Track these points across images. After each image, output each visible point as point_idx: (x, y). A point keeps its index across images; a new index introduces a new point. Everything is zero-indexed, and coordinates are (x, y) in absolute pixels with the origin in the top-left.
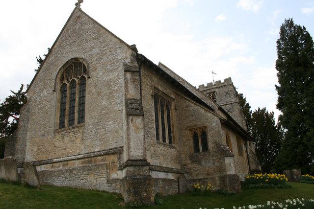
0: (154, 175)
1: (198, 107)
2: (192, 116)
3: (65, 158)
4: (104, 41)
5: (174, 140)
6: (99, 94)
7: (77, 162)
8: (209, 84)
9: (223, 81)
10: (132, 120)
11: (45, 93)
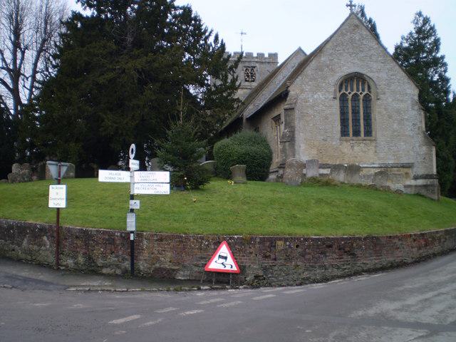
6: (390, 117)
8: (248, 53)
9: (266, 56)
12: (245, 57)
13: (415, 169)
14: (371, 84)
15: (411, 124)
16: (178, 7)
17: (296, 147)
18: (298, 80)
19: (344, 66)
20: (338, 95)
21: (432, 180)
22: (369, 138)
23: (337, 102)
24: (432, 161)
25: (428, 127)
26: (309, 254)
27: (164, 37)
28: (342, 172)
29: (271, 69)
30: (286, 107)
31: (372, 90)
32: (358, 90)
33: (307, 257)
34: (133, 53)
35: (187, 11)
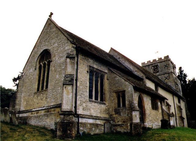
0: (81, 120)
1: (121, 78)
2: (117, 84)
3: (37, 109)
4: (60, 39)
5: (105, 99)
7: (43, 112)
10: (65, 88)
11: (31, 70)
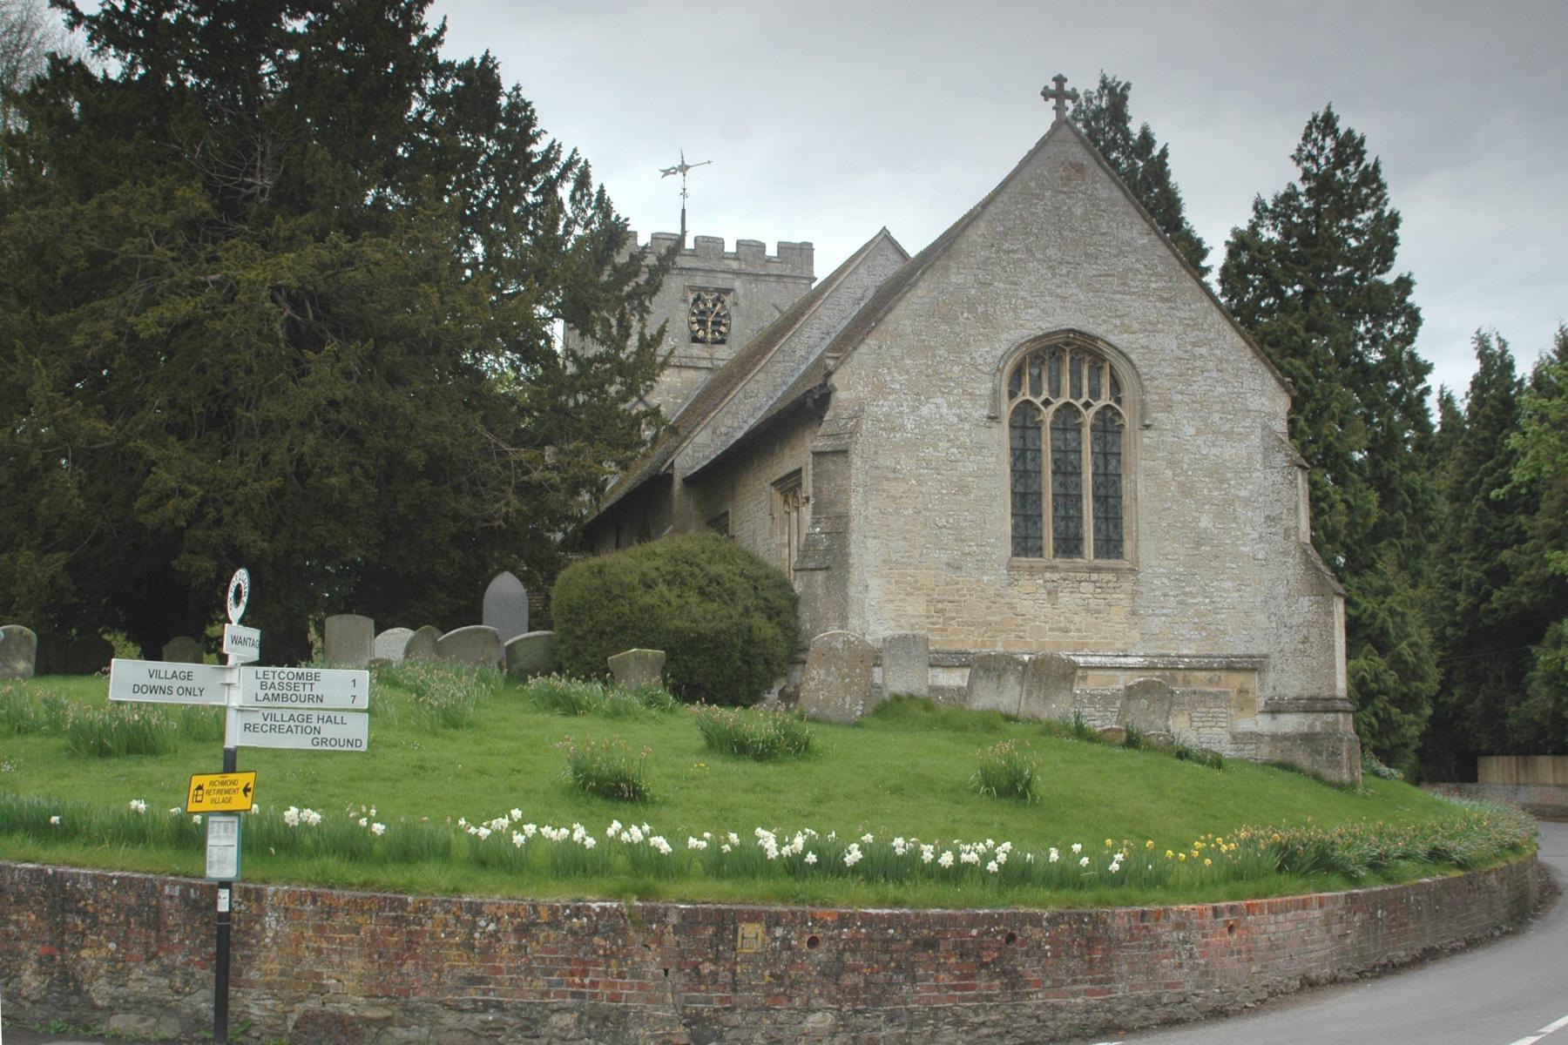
6: (1186, 490)
9: (730, 248)
12: (693, 253)
13: (1271, 677)
14: (1123, 371)
15: (1259, 518)
16: (450, 65)
17: (852, 591)
18: (865, 351)
19: (1029, 305)
20: (1006, 409)
21: (1330, 717)
22: (1112, 563)
23: (1001, 436)
24: (1331, 647)
25: (1324, 537)
26: (855, 969)
27: (391, 173)
28: (1011, 680)
29: (785, 297)
30: (821, 444)
31: (1126, 394)
32: (1077, 393)
33: (849, 980)
34: (272, 231)
35: (481, 77)
